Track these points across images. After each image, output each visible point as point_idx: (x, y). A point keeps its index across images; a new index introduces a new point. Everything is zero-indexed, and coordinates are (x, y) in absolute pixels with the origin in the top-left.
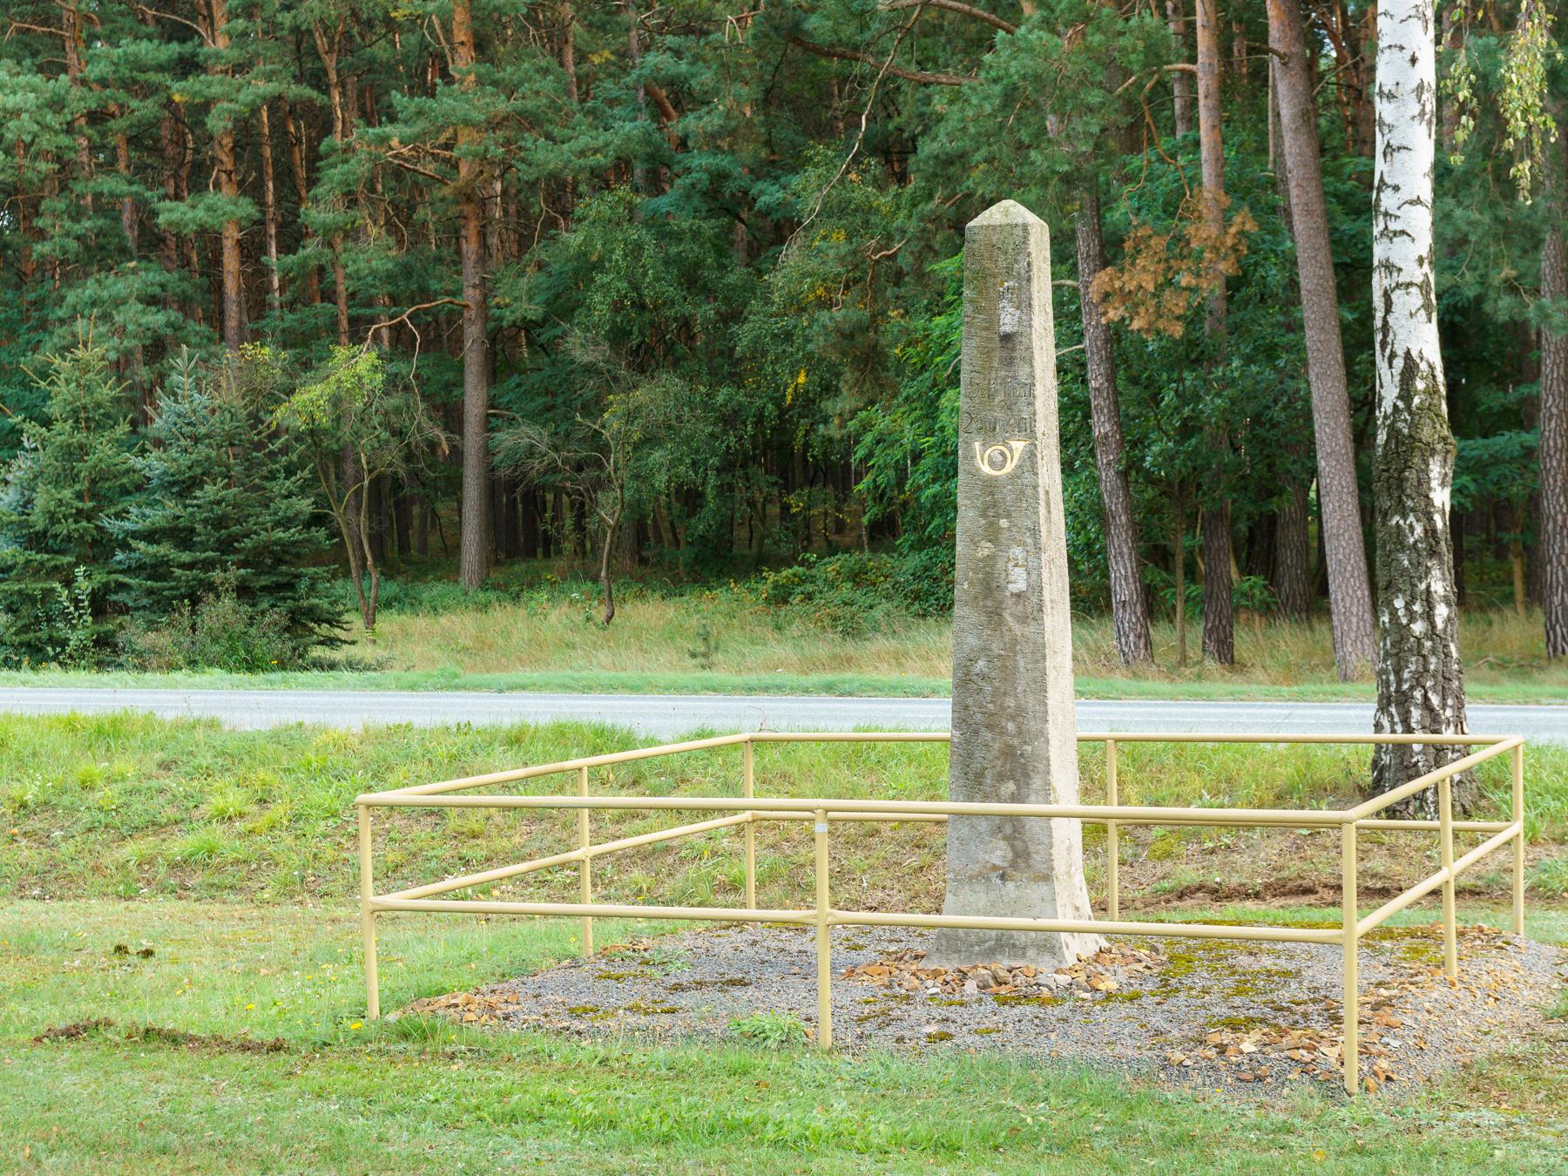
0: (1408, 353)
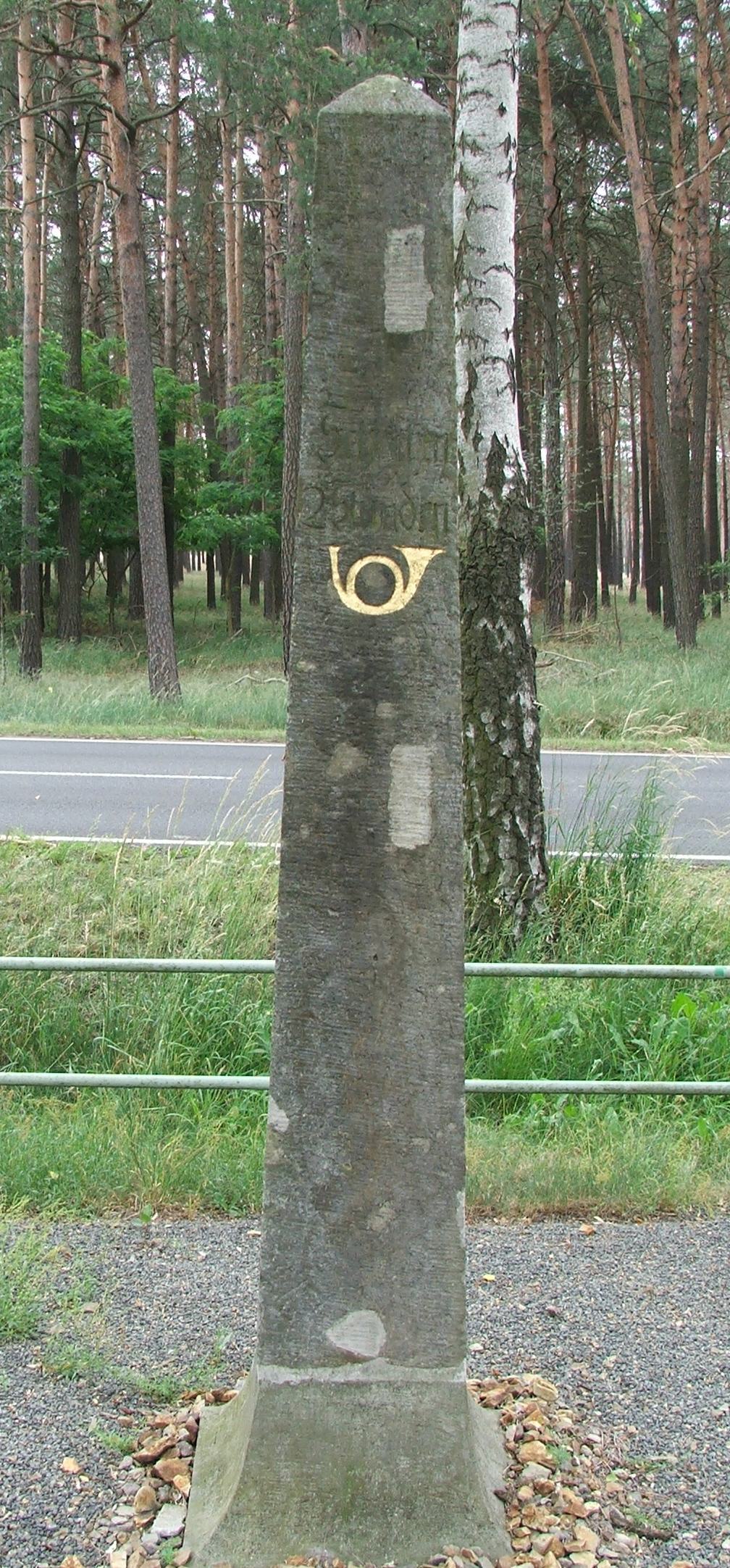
0: (495, 436)
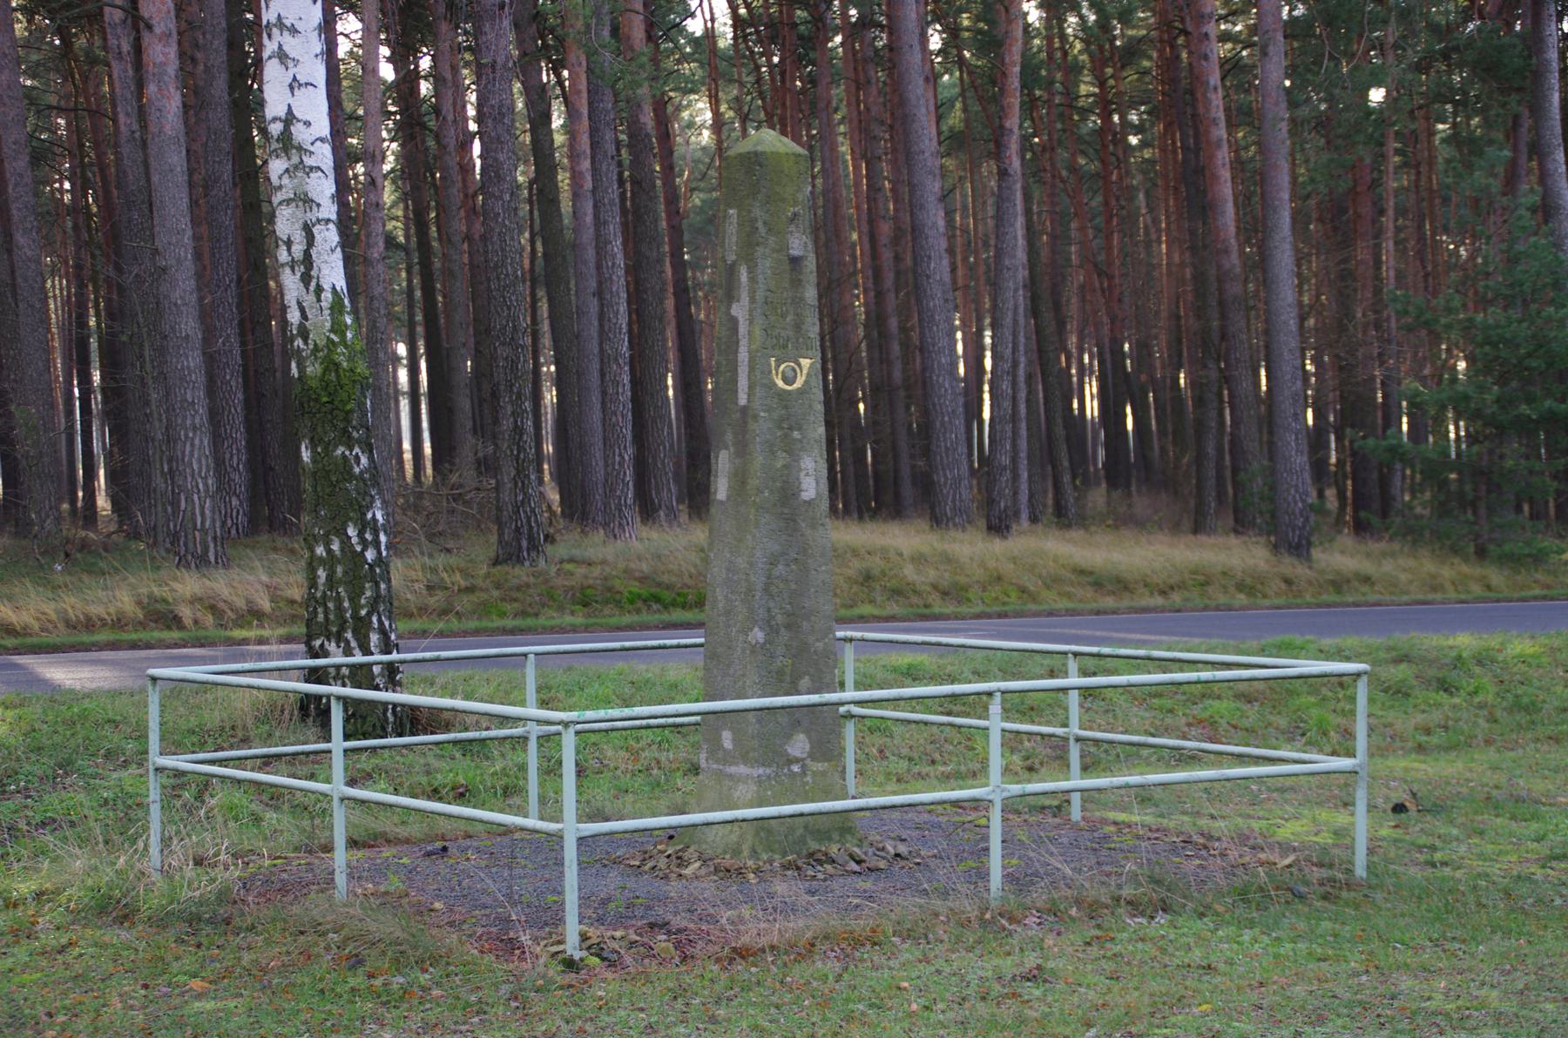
0: (334, 288)
